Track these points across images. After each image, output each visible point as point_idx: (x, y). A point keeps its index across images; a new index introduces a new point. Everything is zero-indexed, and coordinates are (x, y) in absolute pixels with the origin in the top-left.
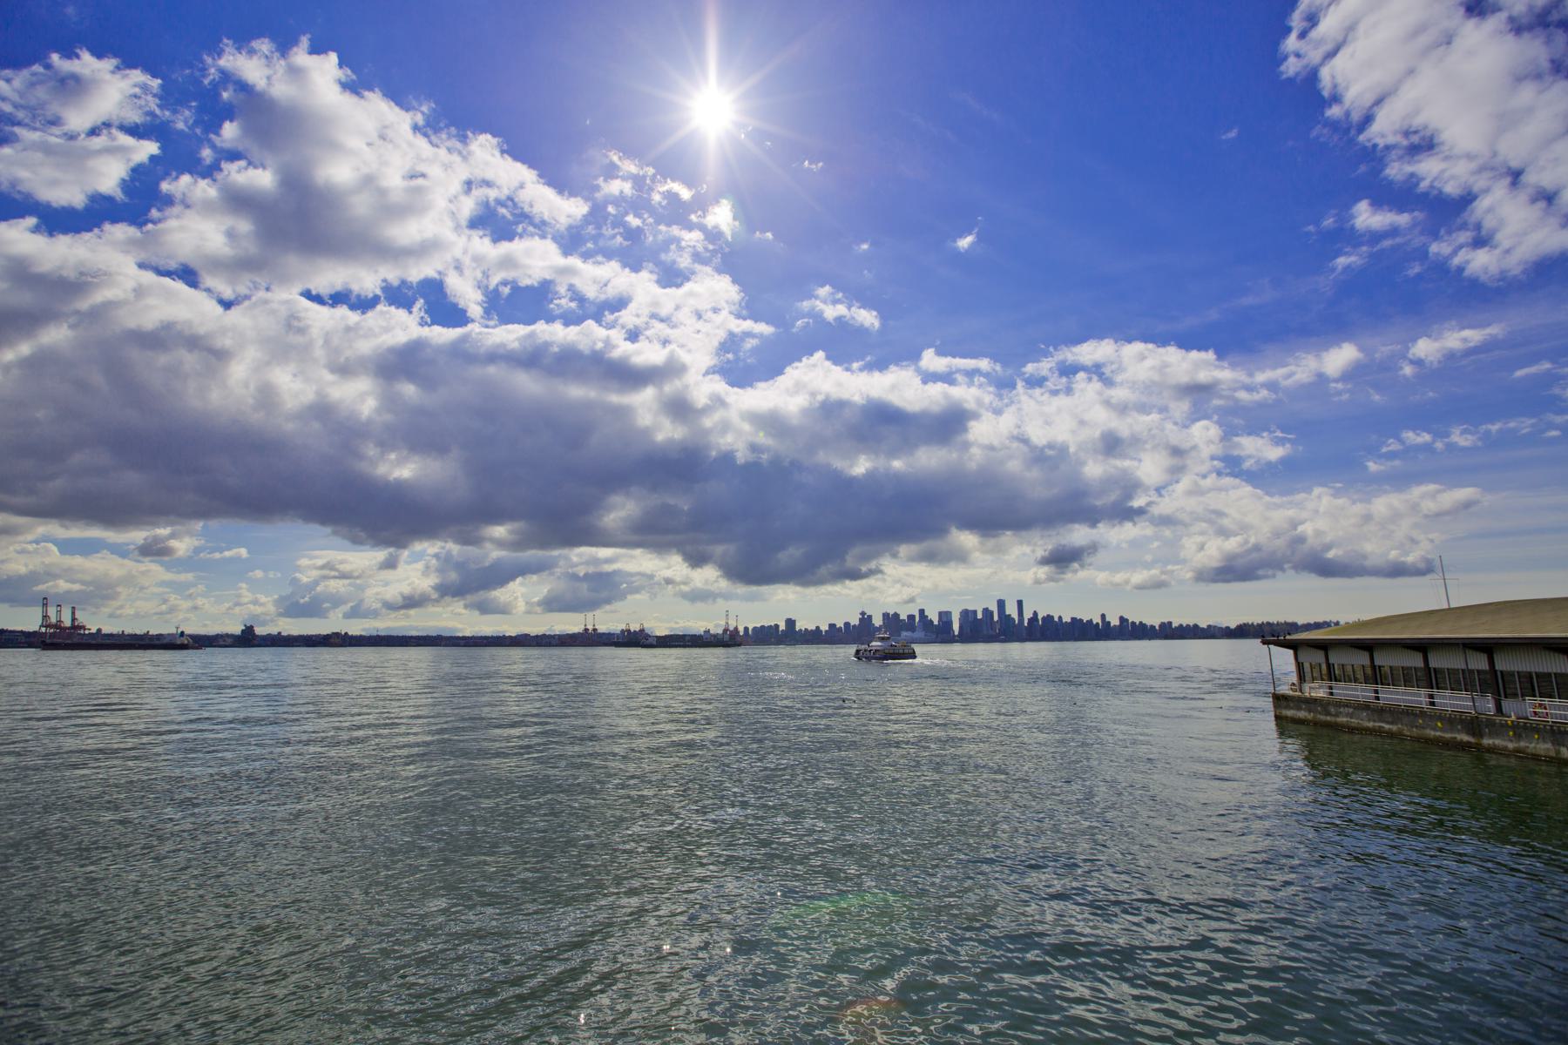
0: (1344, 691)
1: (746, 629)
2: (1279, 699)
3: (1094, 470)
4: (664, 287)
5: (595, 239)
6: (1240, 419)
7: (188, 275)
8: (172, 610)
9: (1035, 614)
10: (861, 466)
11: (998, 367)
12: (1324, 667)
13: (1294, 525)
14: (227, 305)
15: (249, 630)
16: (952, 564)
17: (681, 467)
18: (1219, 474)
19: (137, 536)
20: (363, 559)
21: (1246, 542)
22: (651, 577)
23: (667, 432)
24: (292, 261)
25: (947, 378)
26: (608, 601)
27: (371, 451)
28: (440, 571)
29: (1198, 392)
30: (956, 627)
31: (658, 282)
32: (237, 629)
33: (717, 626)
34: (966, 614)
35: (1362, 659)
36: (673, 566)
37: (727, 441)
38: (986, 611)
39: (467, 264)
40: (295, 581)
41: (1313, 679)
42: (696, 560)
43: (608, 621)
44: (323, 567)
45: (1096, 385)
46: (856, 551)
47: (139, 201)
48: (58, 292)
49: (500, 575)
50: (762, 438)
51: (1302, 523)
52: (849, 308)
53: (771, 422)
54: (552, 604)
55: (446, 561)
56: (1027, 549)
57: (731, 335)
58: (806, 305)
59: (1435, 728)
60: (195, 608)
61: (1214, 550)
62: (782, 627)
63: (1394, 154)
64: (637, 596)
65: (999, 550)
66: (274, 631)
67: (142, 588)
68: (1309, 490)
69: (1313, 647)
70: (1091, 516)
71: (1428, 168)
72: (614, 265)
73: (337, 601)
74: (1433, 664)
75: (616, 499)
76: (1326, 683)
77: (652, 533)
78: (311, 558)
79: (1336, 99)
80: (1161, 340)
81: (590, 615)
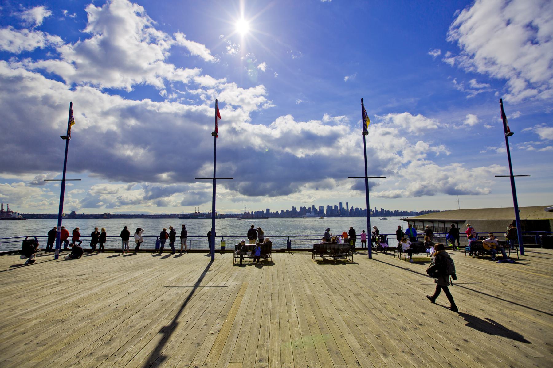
1: (252, 212)
9: (352, 207)
13: (446, 177)
19: (30, 177)
25: (332, 123)
28: (147, 192)
30: (325, 212)
34: (329, 208)
35: (442, 225)
38: (336, 207)
40: (89, 194)
46: (292, 184)
53: (265, 137)
54: (184, 204)
61: (416, 186)
62: (265, 211)
71: (493, 70)
73: (105, 201)
81: (197, 207)
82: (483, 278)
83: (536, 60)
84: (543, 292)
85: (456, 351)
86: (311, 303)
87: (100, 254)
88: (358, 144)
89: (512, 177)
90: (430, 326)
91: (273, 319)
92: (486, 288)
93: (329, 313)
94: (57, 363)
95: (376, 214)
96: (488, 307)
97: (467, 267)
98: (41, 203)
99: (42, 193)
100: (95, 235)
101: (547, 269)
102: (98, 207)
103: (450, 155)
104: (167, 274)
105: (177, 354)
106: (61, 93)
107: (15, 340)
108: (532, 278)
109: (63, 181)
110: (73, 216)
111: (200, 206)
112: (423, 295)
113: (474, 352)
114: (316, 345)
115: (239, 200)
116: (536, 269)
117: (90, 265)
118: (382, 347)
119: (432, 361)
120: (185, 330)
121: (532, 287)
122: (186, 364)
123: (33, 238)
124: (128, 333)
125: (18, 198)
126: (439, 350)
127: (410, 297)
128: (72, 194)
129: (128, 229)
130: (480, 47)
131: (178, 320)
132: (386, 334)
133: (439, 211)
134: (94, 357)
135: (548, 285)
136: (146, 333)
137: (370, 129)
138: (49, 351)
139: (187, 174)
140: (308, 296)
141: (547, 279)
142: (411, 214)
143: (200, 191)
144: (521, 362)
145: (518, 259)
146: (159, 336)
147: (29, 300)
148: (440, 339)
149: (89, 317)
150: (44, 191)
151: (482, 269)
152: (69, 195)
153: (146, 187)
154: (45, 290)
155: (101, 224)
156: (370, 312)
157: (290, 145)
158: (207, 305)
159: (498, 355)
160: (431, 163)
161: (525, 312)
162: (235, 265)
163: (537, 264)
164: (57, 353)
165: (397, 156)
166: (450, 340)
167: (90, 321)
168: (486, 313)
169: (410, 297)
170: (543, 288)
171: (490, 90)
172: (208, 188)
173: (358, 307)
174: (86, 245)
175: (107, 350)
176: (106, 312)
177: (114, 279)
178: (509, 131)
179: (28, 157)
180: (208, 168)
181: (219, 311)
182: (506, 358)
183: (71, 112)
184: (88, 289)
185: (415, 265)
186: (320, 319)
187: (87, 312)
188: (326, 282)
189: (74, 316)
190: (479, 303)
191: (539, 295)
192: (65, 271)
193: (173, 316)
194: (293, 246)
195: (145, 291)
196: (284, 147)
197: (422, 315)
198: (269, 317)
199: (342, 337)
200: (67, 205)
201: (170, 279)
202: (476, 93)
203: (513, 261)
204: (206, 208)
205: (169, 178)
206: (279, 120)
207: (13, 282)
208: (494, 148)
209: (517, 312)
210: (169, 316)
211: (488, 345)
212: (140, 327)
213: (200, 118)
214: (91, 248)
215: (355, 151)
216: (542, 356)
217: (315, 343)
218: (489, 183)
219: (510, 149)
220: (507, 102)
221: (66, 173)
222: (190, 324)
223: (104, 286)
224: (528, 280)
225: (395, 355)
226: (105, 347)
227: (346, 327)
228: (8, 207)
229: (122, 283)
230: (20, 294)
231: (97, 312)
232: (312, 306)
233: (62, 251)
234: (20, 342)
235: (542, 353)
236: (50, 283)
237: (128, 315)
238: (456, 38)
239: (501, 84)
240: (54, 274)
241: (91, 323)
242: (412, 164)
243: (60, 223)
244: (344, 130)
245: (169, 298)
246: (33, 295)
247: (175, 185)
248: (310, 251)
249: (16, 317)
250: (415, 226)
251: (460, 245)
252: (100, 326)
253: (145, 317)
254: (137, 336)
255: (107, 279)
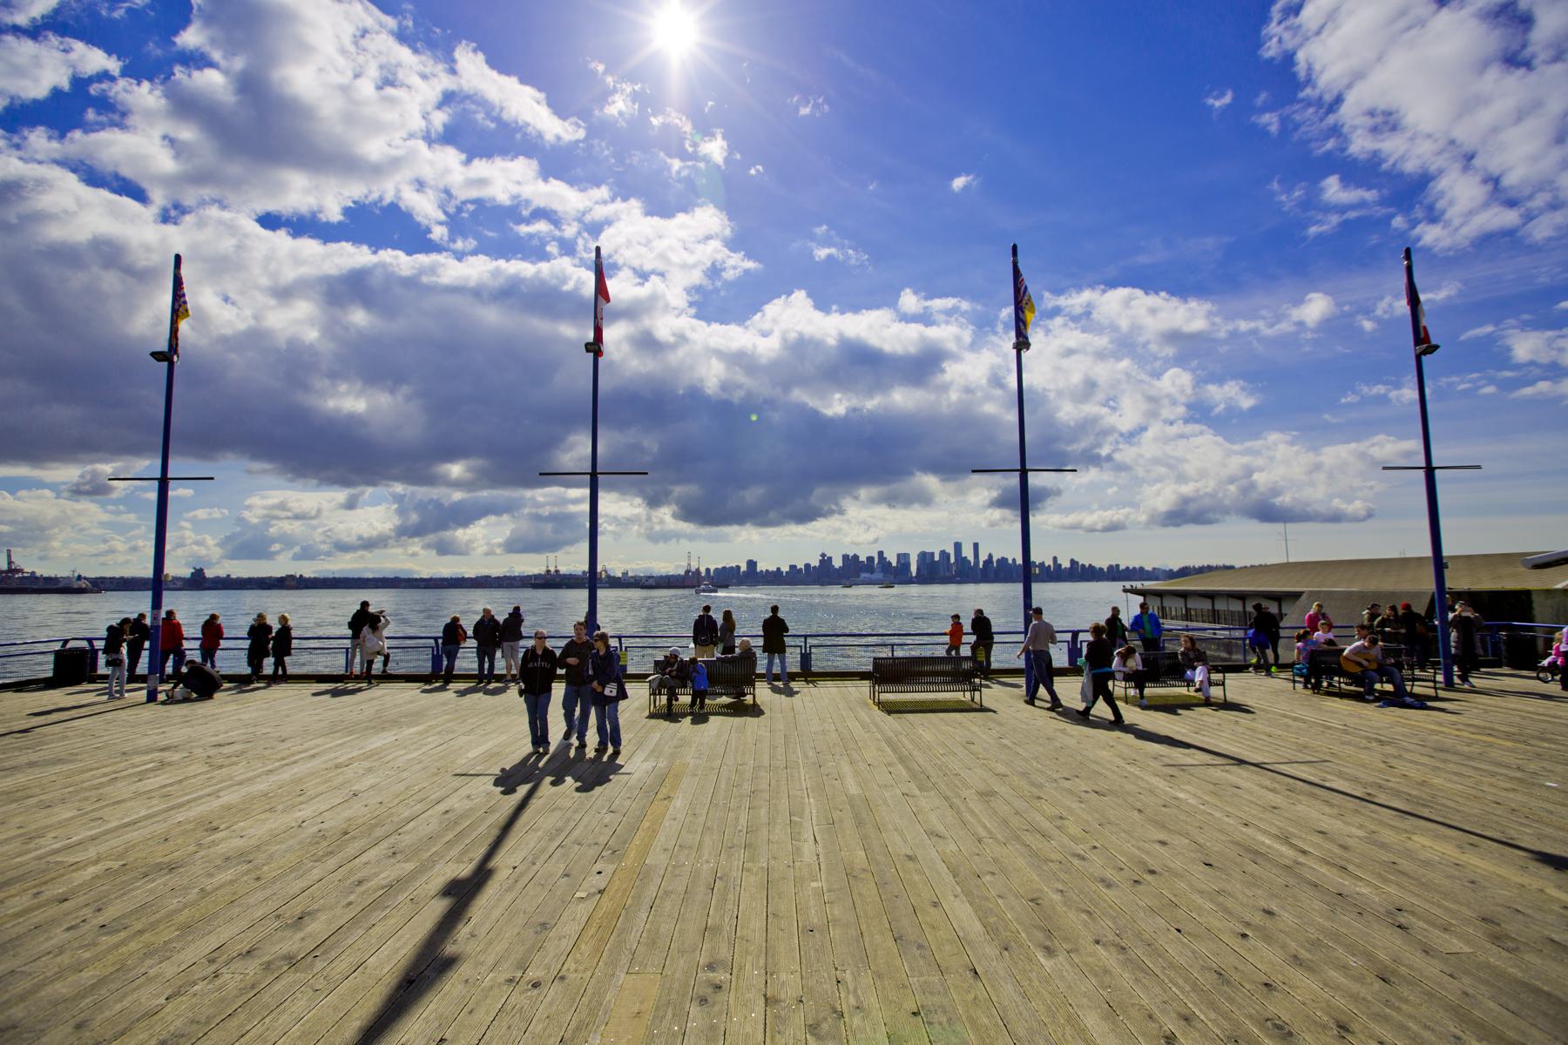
1: (708, 570)
9: (990, 556)
11: (979, 307)
13: (1249, 471)
16: (916, 506)
17: (658, 404)
19: (69, 473)
25: (925, 319)
28: (401, 512)
30: (914, 569)
34: (924, 557)
35: (1206, 605)
38: (944, 554)
39: (426, 179)
40: (241, 521)
46: (820, 491)
49: (464, 516)
53: (740, 360)
61: (1163, 497)
62: (744, 568)
63: (1359, 132)
65: (963, 492)
66: (222, 573)
71: (1391, 146)
73: (287, 541)
79: (1309, 81)
81: (551, 556)
82: (1335, 749)
83: (1520, 116)
84: (1491, 785)
85: (1239, 940)
86: (856, 816)
87: (275, 687)
88: (996, 381)
89: (1430, 471)
90: (1176, 875)
91: (752, 859)
92: (1341, 775)
93: (905, 842)
94: (156, 976)
95: (1056, 574)
96: (1339, 824)
97: (1295, 719)
98: (103, 547)
99: (105, 517)
100: (259, 631)
101: (1511, 725)
102: (270, 556)
103: (1254, 412)
104: (463, 739)
105: (483, 951)
106: (139, 230)
107: (37, 917)
108: (1466, 749)
109: (163, 483)
110: (197, 582)
111: (560, 554)
112: (1166, 794)
113: (1288, 941)
114: (864, 927)
115: (666, 537)
116: (1481, 723)
117: (243, 717)
118: (1042, 929)
119: (1172, 966)
120: (509, 890)
121: (1464, 771)
122: (509, 976)
123: (85, 644)
124: (352, 898)
125: (33, 531)
126: (1196, 936)
127: (1131, 800)
128: (194, 521)
129: (781, 615)
130: (1358, 76)
131: (492, 864)
132: (1056, 897)
133: (1232, 568)
134: (258, 961)
135: (1508, 767)
136: (400, 898)
137: (1035, 337)
138: (133, 946)
139: (523, 464)
140: (851, 799)
141: (1508, 749)
142: (1139, 574)
143: (556, 510)
144: (1410, 967)
145: (1437, 699)
146: (440, 907)
147: (76, 813)
148: (1200, 909)
149: (243, 856)
150: (111, 512)
151: (1334, 723)
152: (184, 524)
153: (399, 499)
154: (120, 785)
155: (274, 607)
156: (1018, 838)
157: (803, 382)
158: (572, 824)
159: (1351, 948)
160: (1201, 433)
161: (1437, 837)
162: (652, 716)
163: (1486, 711)
164: (156, 951)
165: (1105, 410)
166: (1226, 910)
167: (245, 867)
168: (1333, 841)
169: (1131, 800)
170: (1493, 774)
171: (1382, 211)
172: (576, 501)
173: (985, 827)
174: (232, 659)
175: (292, 943)
176: (291, 842)
177: (313, 756)
178: (1427, 339)
179: (63, 414)
180: (576, 451)
181: (602, 840)
182: (1369, 957)
183: (178, 283)
184: (240, 783)
185: (1152, 713)
186: (880, 858)
187: (237, 843)
188: (902, 760)
189: (202, 853)
190: (1315, 814)
191: (1480, 794)
192: (177, 734)
193: (479, 853)
194: (816, 667)
195: (401, 786)
196: (787, 387)
197: (1157, 846)
198: (741, 854)
199: (935, 905)
200: (180, 552)
201: (471, 755)
202: (1335, 219)
203: (1420, 703)
204: (574, 561)
205: (469, 475)
206: (773, 309)
207: (31, 764)
208: (1380, 389)
209: (1415, 838)
210: (464, 852)
211: (1326, 924)
212: (384, 883)
213: (546, 299)
214: (248, 671)
215: (988, 398)
216: (1467, 949)
217: (862, 921)
218: (1371, 488)
219: (1427, 391)
220: (1427, 250)
221: (170, 462)
222: (522, 874)
223: (286, 775)
224: (1456, 753)
225: (1076, 950)
226: (288, 933)
227: (949, 878)
228: (9, 556)
229: (337, 767)
230: (51, 795)
231: (267, 843)
232: (859, 824)
233: (164, 680)
234: (53, 922)
235: (1468, 942)
236: (134, 766)
237: (351, 850)
238: (1289, 44)
239: (1411, 192)
240: (143, 742)
241: (248, 872)
242: (1149, 434)
243: (157, 604)
244: (958, 339)
245: (467, 804)
246: (87, 799)
247: (485, 494)
248: (863, 676)
249: (40, 858)
250: (1163, 608)
251: (1281, 661)
252: (275, 880)
253: (399, 857)
254: (375, 905)
255: (293, 755)
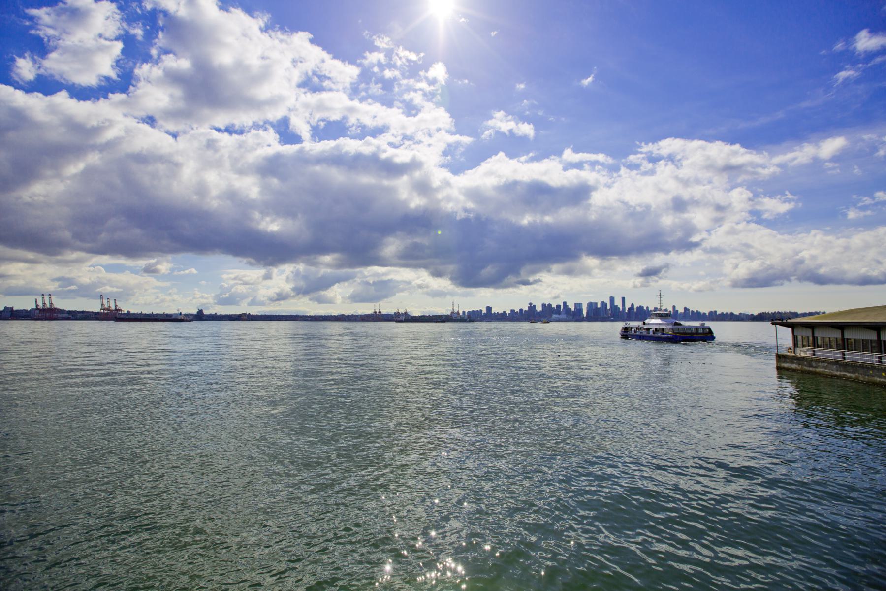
0: (821, 353)
1: (464, 312)
2: (779, 357)
3: (668, 220)
4: (407, 116)
5: (366, 90)
6: (763, 187)
7: (150, 120)
8: (163, 301)
9: (632, 305)
10: (526, 220)
12: (811, 338)
14: (175, 136)
15: (200, 312)
17: (419, 222)
18: (748, 222)
19: (142, 263)
20: (255, 273)
21: (764, 263)
22: (409, 283)
23: (416, 202)
24: (206, 112)
25: (579, 166)
26: (386, 297)
27: (257, 215)
29: (730, 169)
30: (585, 313)
31: (280, 142)
32: (194, 311)
33: (447, 310)
34: (591, 306)
35: (837, 334)
36: (423, 277)
37: (449, 207)
38: (604, 304)
40: (221, 287)
41: (803, 346)
42: (437, 274)
43: (387, 307)
44: (235, 279)
45: (671, 167)
46: (528, 267)
47: (122, 83)
48: (82, 137)
49: (326, 283)
50: (470, 205)
51: (801, 251)
52: (517, 124)
53: (474, 194)
54: (356, 298)
55: (297, 274)
56: (626, 268)
57: (449, 145)
58: (491, 123)
59: (880, 377)
60: (174, 300)
61: (744, 269)
62: (484, 311)
64: (401, 294)
67: (146, 290)
68: (808, 232)
69: (803, 327)
70: (666, 248)
72: (378, 105)
73: (244, 297)
74: (846, 337)
75: (391, 239)
76: (811, 348)
77: (411, 258)
78: (228, 274)
80: (710, 139)
81: (377, 304)
103: (791, 213)
